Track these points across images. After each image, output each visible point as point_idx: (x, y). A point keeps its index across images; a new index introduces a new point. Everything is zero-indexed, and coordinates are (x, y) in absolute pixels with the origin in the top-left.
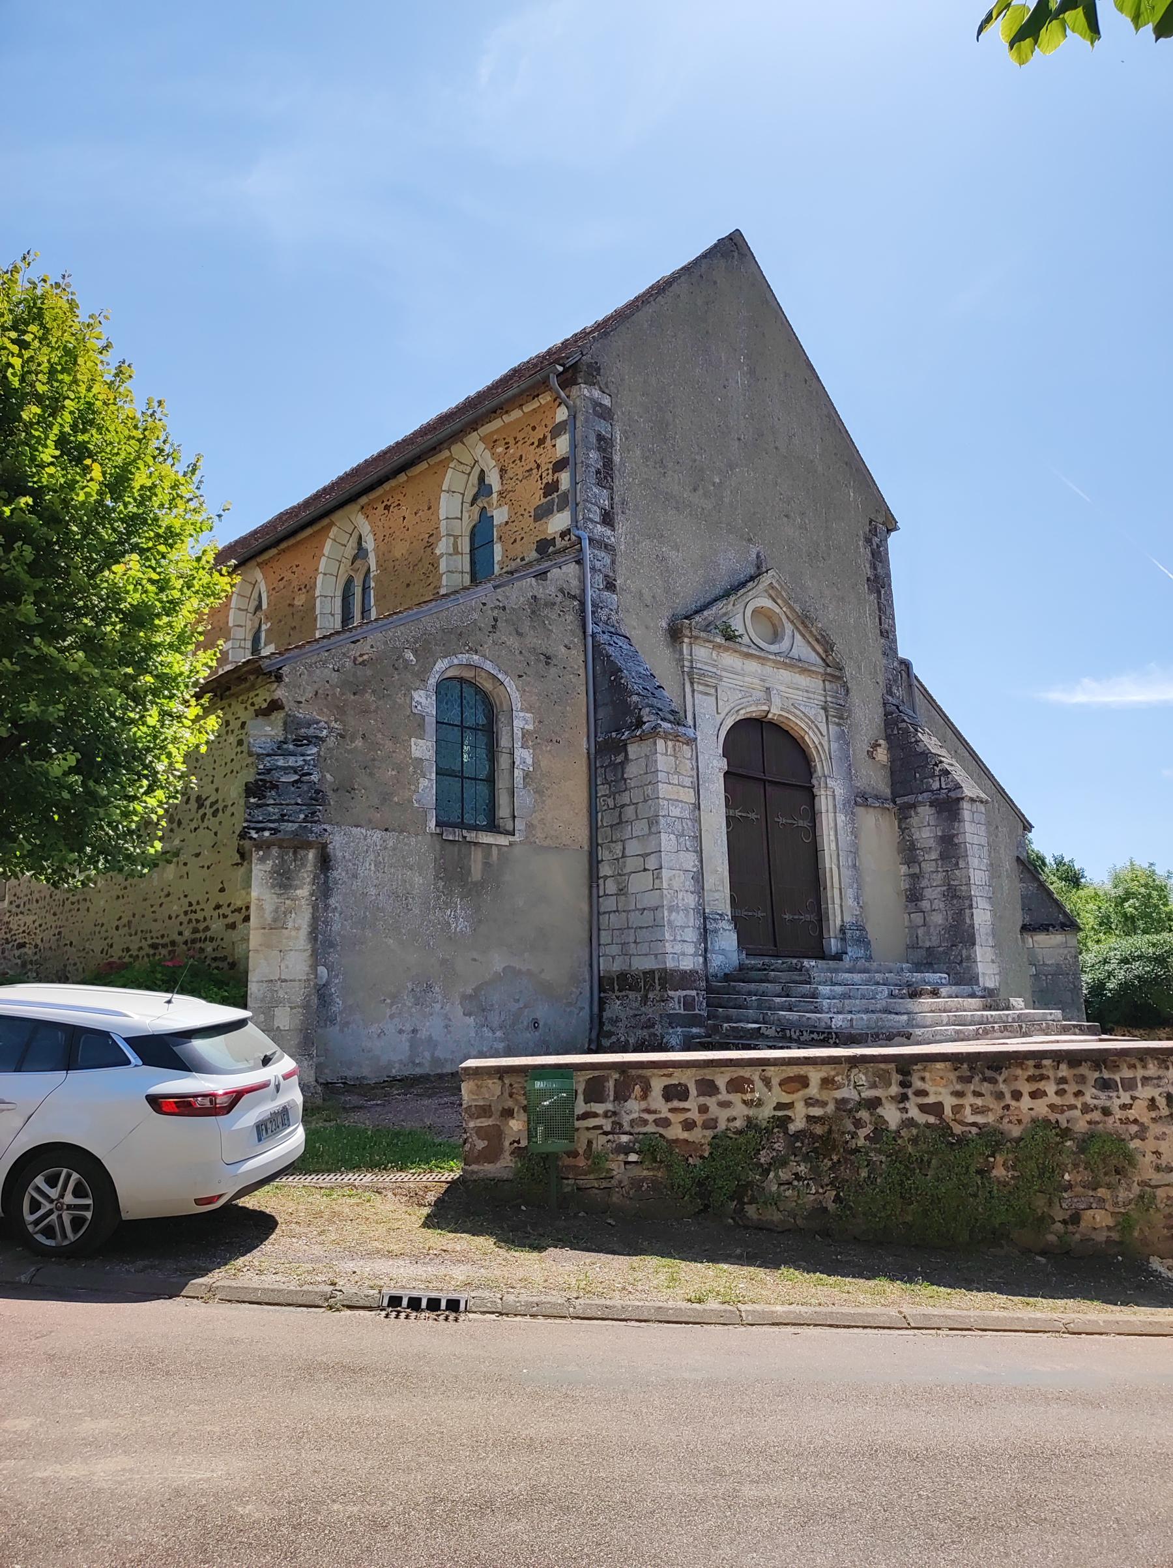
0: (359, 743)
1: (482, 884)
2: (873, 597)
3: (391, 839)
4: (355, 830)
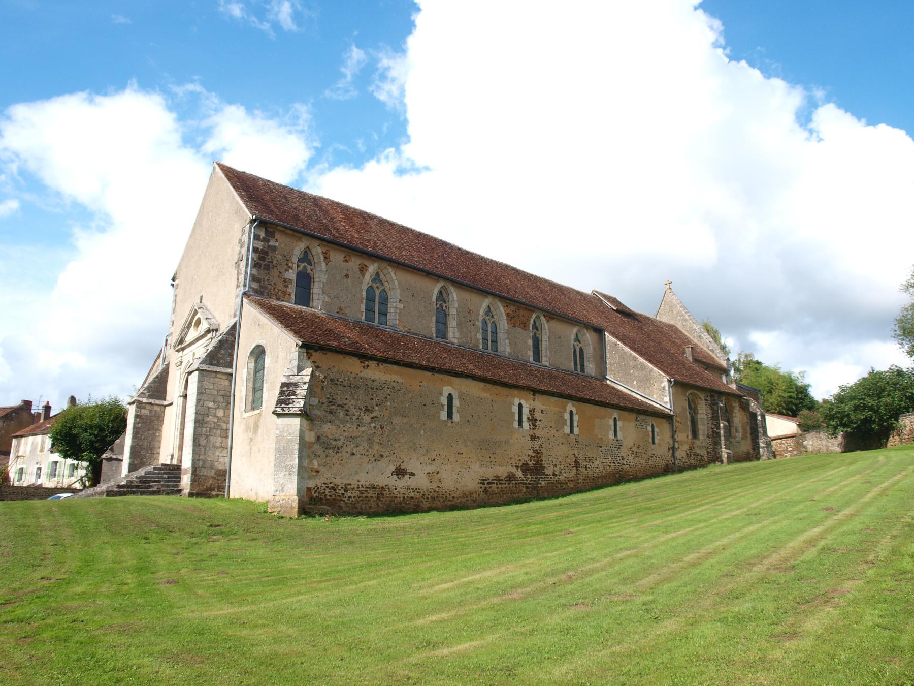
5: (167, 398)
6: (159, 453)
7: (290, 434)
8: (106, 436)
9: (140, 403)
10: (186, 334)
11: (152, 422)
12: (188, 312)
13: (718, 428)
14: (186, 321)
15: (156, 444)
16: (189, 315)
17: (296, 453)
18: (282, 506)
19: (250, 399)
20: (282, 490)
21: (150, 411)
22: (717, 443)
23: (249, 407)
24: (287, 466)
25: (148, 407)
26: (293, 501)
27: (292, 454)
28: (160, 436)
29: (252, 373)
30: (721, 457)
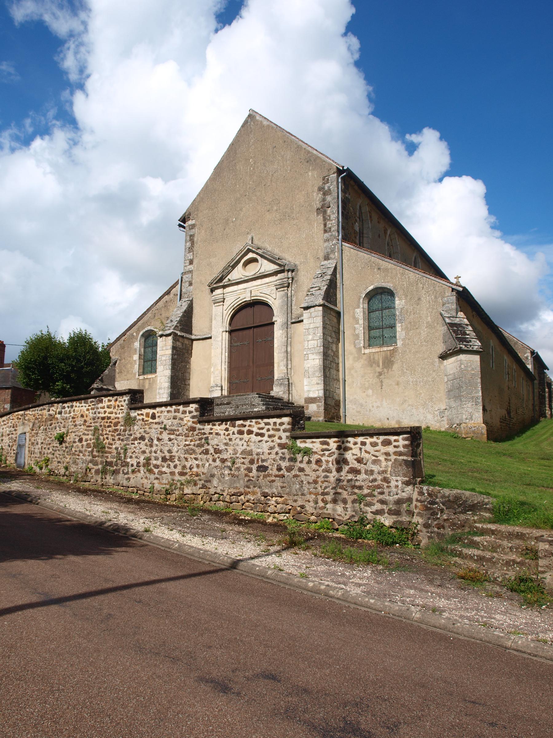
0: (123, 360)
1: (148, 389)
2: (321, 217)
3: (129, 382)
4: (122, 382)
5: (194, 332)
6: (189, 385)
7: (473, 369)
8: (82, 367)
9: (175, 335)
10: (229, 273)
11: (184, 354)
12: (236, 250)
13: (544, 392)
14: (233, 260)
15: (187, 375)
16: (237, 254)
17: (479, 386)
18: (474, 432)
19: (367, 337)
20: (471, 418)
21: (182, 344)
22: (542, 403)
23: (367, 345)
24: (472, 398)
25: (181, 339)
26: (482, 428)
27: (476, 388)
28: (189, 368)
29: (367, 312)
30: (545, 413)
